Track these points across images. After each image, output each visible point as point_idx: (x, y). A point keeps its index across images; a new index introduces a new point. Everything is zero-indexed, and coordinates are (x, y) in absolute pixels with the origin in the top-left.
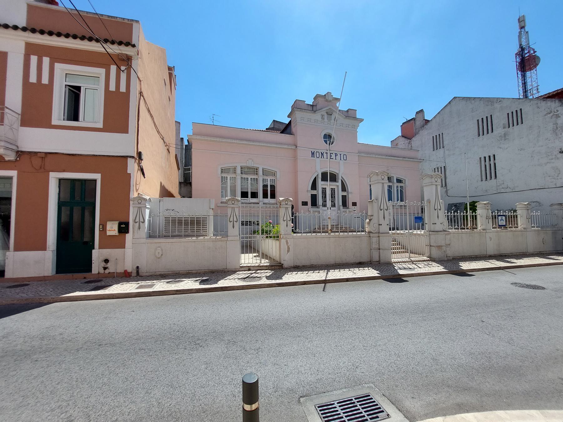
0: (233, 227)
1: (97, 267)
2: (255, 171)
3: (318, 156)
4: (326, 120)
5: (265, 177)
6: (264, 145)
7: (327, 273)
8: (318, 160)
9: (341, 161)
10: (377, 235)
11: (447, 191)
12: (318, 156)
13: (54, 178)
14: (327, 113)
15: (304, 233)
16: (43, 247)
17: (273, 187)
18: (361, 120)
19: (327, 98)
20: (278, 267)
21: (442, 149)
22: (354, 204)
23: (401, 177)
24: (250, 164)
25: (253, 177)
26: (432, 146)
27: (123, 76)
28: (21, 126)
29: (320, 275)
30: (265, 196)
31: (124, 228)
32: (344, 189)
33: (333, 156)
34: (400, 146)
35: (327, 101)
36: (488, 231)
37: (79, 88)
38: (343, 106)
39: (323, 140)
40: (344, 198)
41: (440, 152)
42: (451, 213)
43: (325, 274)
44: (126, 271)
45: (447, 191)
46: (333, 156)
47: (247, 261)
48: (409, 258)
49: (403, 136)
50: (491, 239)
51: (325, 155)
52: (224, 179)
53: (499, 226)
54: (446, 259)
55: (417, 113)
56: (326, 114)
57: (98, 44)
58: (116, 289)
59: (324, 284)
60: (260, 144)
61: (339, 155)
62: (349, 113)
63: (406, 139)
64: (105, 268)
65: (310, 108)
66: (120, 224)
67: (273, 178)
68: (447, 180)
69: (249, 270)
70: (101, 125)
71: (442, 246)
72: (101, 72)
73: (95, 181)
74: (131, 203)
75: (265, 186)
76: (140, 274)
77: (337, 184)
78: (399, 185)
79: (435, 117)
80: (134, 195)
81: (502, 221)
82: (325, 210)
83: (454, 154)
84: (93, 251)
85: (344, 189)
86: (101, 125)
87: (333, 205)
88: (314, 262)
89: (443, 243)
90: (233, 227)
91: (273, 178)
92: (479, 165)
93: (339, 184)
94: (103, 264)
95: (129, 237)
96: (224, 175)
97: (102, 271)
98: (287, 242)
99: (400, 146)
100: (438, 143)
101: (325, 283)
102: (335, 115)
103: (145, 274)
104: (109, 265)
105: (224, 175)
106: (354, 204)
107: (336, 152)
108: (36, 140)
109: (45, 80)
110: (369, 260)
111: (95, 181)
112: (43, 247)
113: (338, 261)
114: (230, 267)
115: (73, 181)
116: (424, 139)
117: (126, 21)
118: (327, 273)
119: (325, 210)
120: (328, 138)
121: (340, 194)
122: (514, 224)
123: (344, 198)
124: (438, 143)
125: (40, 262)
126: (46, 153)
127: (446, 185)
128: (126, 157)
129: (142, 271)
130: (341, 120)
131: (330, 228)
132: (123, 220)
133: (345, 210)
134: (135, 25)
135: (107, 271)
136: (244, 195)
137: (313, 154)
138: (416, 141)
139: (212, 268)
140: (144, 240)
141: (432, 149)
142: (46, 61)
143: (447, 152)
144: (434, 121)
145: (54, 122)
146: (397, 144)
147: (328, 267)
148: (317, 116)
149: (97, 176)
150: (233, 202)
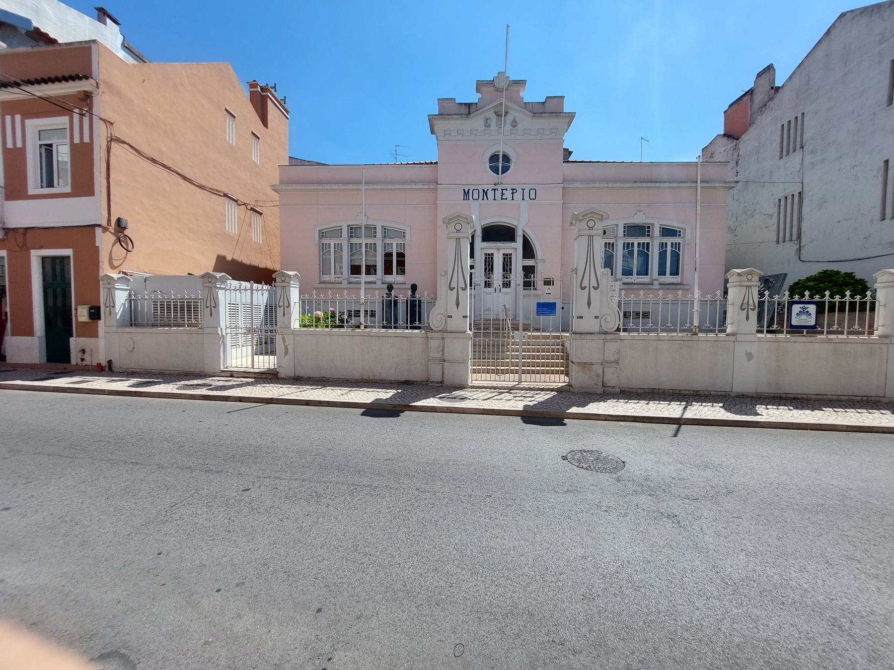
0: (747, 318)
1: (75, 359)
2: (371, 230)
3: (476, 197)
4: (494, 126)
5: (388, 241)
6: (383, 187)
7: (685, 408)
8: (475, 204)
9: (523, 203)
10: (439, 335)
11: (799, 251)
12: (476, 197)
13: (36, 255)
14: (495, 113)
15: (643, 331)
16: (30, 332)
17: (401, 255)
18: (571, 116)
19: (497, 85)
20: (271, 376)
21: (799, 153)
22: (548, 283)
23: (673, 224)
24: (639, 220)
25: (369, 241)
26: (778, 149)
27: (86, 120)
28: (6, 200)
29: (673, 410)
30: (388, 270)
31: (95, 313)
32: (528, 251)
33: (508, 194)
34: (717, 158)
35: (498, 90)
36: (740, 337)
37: (51, 145)
38: (532, 94)
39: (488, 165)
40: (529, 271)
41: (795, 159)
42: (844, 296)
43: (682, 408)
44: (99, 365)
45: (799, 251)
46: (508, 194)
47: (234, 364)
48: (520, 382)
49: (725, 135)
50: (750, 356)
51: (490, 194)
52: (324, 248)
53: (792, 326)
54: (600, 390)
55: (759, 75)
56: (494, 117)
57: (16, 90)
58: (594, 408)
59: (675, 426)
60: (375, 187)
61: (520, 191)
62: (547, 105)
63: (730, 141)
64: (83, 360)
65: (464, 110)
66: (90, 308)
67: (400, 241)
68: (804, 225)
69: (232, 376)
70: (68, 189)
71: (592, 364)
72: (63, 121)
73: (44, 259)
74: (101, 282)
75: (388, 256)
76: (114, 369)
77: (513, 244)
78: (669, 240)
79: (790, 78)
80: (101, 274)
81: (804, 317)
82: (490, 294)
83: (823, 160)
84: (71, 339)
85: (528, 251)
86: (68, 189)
87: (507, 285)
88: (326, 373)
89: (596, 357)
90: (747, 318)
91: (400, 241)
92: (880, 179)
93: (519, 244)
94: (80, 355)
95: (101, 323)
96: (325, 241)
97: (80, 363)
98: (283, 339)
99: (717, 158)
100: (792, 139)
101: (680, 425)
102: (516, 113)
103: (118, 370)
104: (85, 356)
105: (325, 241)
106: (548, 283)
107: (514, 187)
108: (22, 214)
109: (86, 139)
110: (424, 378)
111: (69, 257)
112: (30, 332)
113: (367, 375)
114: (208, 369)
115: (54, 259)
116: (766, 130)
117: (84, 45)
118: (685, 408)
119: (490, 294)
120: (499, 163)
121: (518, 263)
122: (189, 319)
123: (529, 271)
124: (792, 139)
125: (26, 347)
126: (26, 229)
127: (799, 237)
128: (93, 226)
129: (116, 365)
130: (525, 121)
131: (696, 323)
132: (95, 304)
133: (527, 292)
134: (93, 46)
135: (84, 363)
136: (355, 270)
137: (466, 194)
138: (748, 142)
139: (187, 369)
140: (114, 329)
141: (778, 155)
142: (18, 118)
143: (808, 158)
144: (785, 88)
145: (31, 192)
146: (712, 154)
147: (688, 396)
148: (476, 122)
149: (68, 252)
150: (750, 277)
